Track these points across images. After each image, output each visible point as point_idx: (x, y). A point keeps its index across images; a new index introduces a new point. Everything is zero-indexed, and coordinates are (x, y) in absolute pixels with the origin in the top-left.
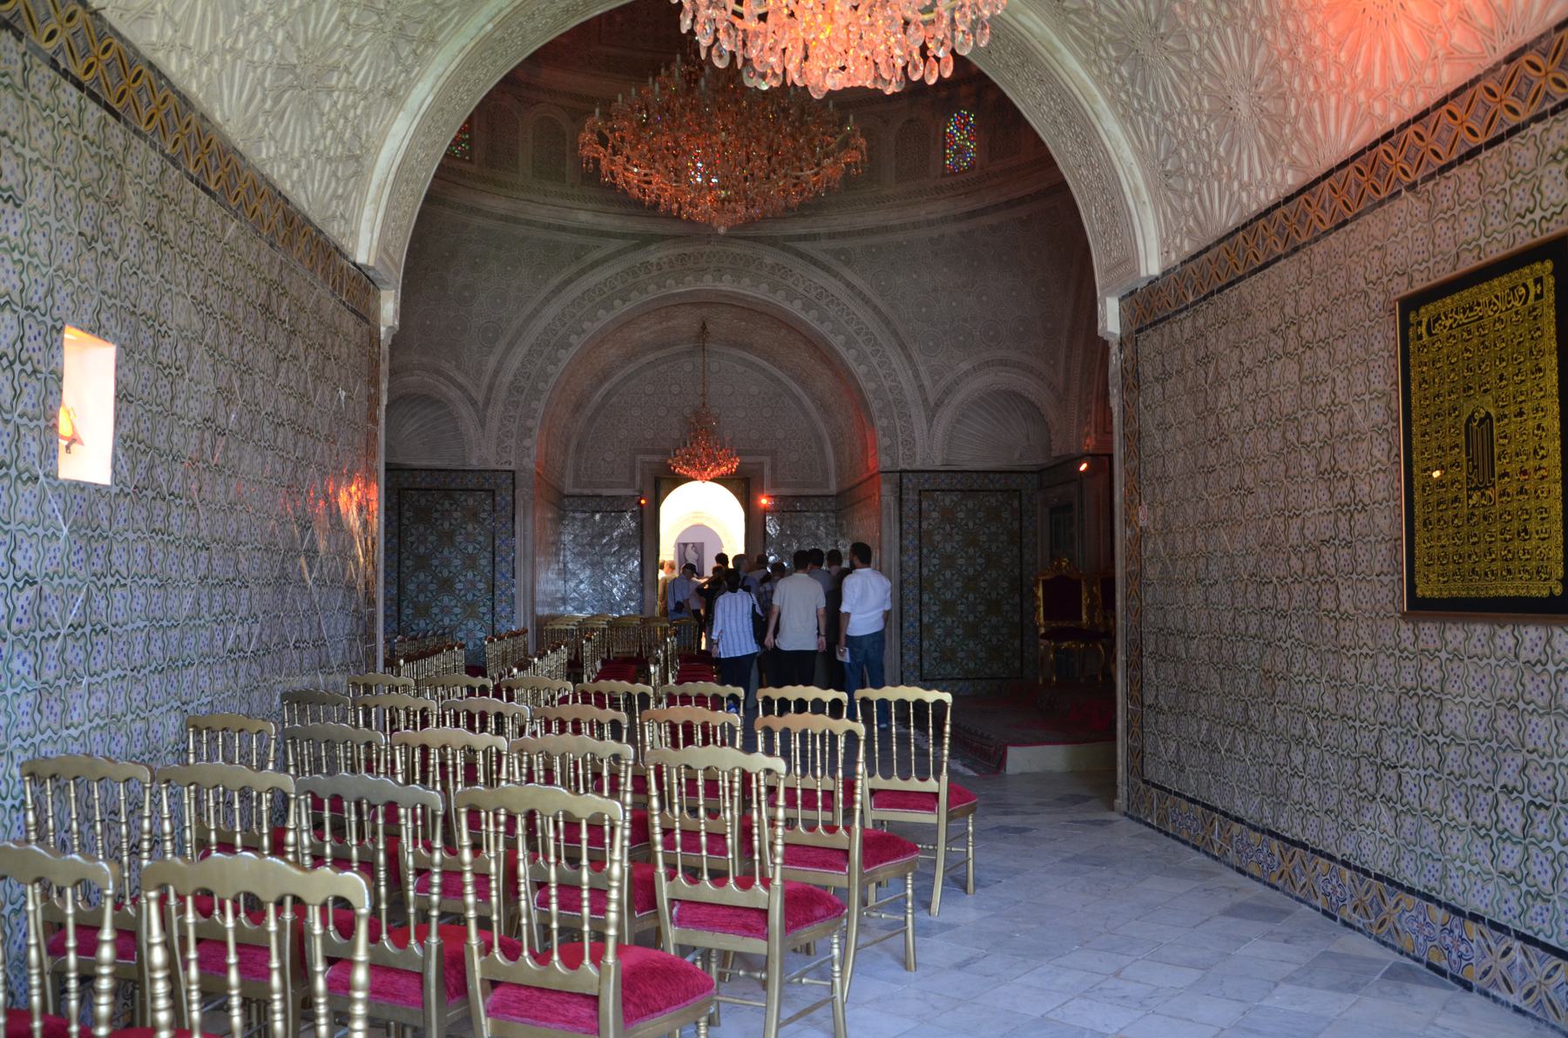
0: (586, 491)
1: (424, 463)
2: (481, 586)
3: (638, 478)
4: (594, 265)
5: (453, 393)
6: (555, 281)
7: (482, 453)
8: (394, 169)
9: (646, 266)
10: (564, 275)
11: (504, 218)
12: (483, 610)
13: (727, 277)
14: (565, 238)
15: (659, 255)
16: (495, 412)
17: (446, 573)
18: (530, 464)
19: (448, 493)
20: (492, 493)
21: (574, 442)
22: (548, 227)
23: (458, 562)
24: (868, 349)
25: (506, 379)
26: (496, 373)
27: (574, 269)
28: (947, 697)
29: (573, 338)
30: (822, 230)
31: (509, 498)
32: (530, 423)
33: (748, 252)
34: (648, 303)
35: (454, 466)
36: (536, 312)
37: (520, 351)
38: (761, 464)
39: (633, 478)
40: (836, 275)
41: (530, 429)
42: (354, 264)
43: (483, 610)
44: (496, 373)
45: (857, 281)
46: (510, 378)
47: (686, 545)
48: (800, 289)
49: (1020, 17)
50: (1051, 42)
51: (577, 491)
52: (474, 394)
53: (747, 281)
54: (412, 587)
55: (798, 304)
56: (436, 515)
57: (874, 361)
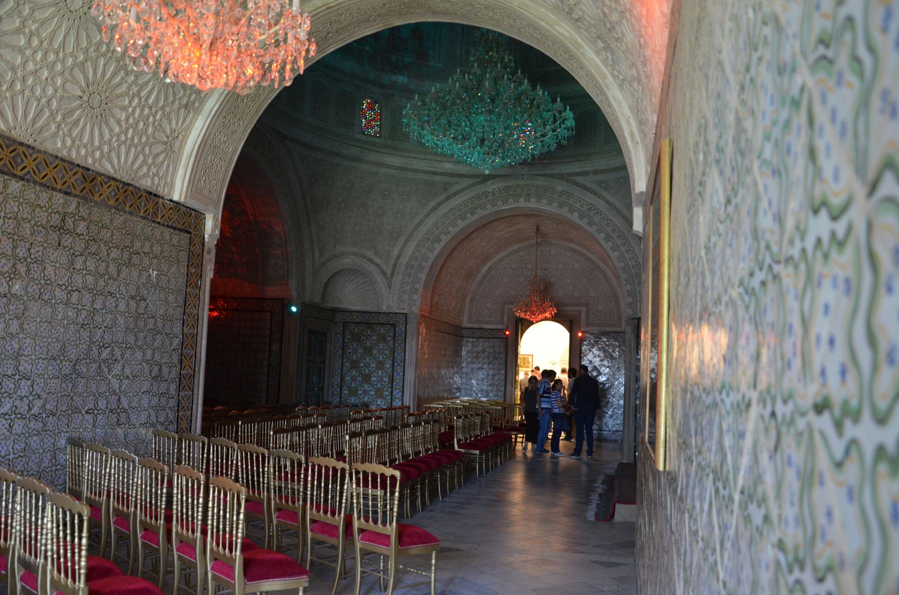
0: (475, 326)
1: (358, 308)
2: (386, 379)
3: (506, 318)
4: (455, 194)
5: (372, 268)
6: (432, 204)
7: (390, 303)
8: (196, 147)
9: (486, 194)
10: (437, 200)
11: (401, 168)
12: (386, 393)
13: (533, 199)
14: (438, 178)
15: (493, 187)
16: (398, 279)
17: (367, 371)
18: (416, 310)
19: (370, 325)
21: (469, 296)
22: (427, 172)
23: (373, 365)
24: (619, 242)
25: (404, 261)
26: (398, 257)
27: (443, 196)
29: (443, 237)
30: (590, 169)
32: (417, 286)
33: (546, 184)
34: (485, 216)
35: (374, 309)
36: (422, 221)
37: (412, 245)
38: (580, 312)
39: (502, 318)
40: (600, 196)
41: (417, 290)
42: (171, 201)
43: (386, 393)
44: (398, 257)
45: (611, 199)
46: (407, 260)
48: (578, 206)
49: (557, 27)
50: (576, 42)
51: (470, 325)
52: (385, 269)
53: (545, 201)
54: (348, 378)
55: (576, 214)
56: (363, 338)
57: (623, 249)
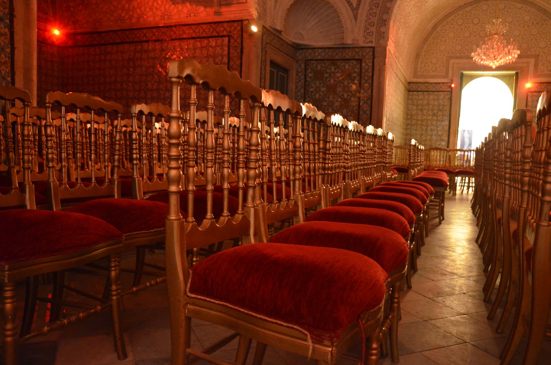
20: (360, 61)
28: (103, 187)
31: (370, 64)
39: (447, 72)
47: (464, 131)
56: (326, 75)
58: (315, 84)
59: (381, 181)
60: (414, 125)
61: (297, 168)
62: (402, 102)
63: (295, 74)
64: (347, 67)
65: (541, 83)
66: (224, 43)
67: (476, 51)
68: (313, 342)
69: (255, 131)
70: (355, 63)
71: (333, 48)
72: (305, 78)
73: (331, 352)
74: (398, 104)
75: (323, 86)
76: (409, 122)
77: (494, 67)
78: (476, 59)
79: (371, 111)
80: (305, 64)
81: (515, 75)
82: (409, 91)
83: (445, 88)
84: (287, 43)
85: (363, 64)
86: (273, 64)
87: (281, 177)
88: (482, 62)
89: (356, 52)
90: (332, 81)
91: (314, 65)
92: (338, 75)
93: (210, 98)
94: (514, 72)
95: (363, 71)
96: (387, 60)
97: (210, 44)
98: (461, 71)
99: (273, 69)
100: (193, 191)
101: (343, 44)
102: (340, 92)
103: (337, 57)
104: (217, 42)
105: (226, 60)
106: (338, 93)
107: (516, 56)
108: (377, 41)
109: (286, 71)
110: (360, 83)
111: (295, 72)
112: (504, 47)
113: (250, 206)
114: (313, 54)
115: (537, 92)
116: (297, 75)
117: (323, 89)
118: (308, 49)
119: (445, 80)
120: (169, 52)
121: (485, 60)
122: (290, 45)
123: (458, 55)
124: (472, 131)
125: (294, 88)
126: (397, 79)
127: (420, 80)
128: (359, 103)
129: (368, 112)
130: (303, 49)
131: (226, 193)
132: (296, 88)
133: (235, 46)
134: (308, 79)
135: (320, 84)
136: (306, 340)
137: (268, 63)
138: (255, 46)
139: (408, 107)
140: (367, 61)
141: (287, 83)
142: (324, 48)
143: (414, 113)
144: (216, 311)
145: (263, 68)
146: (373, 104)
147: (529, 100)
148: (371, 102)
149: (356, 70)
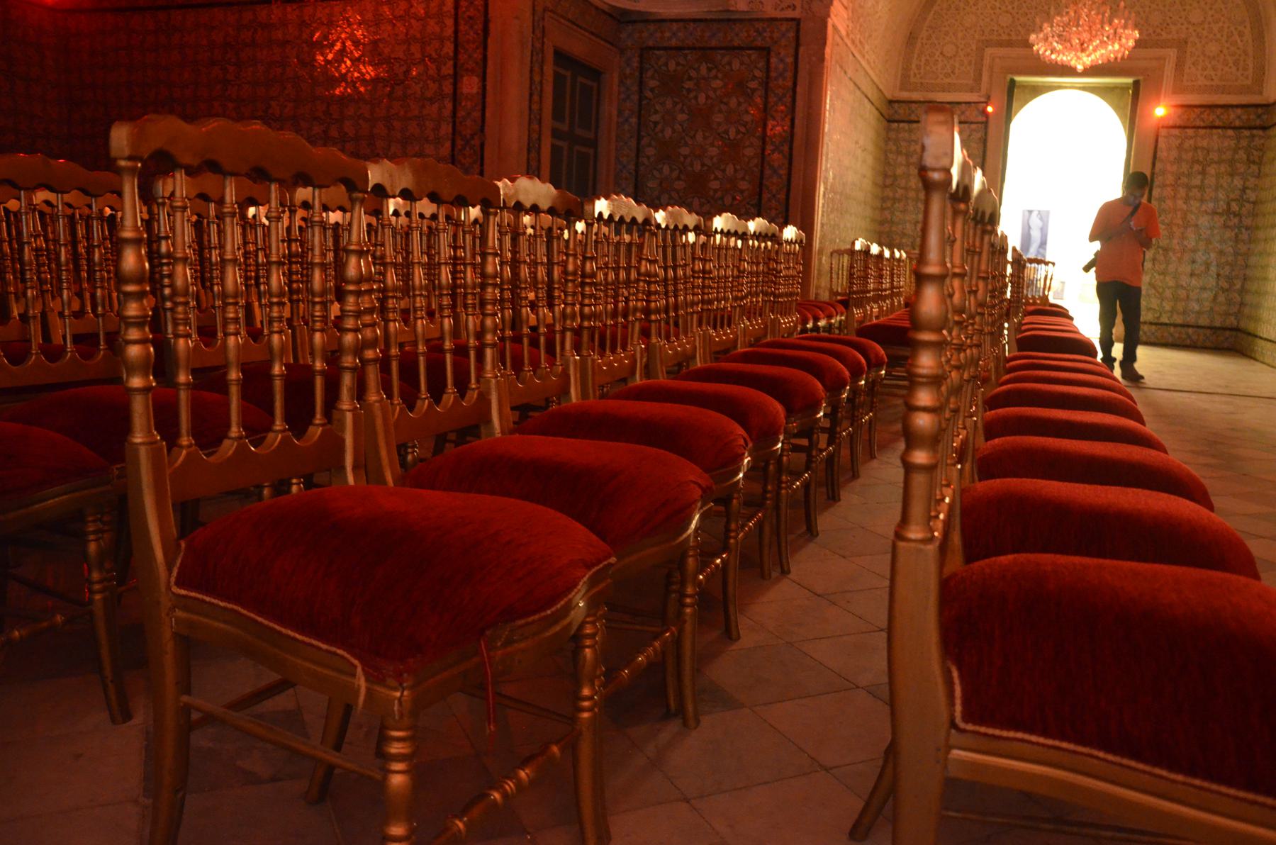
20: (766, 52)
31: (790, 60)
47: (1030, 212)
58: (663, 104)
59: (765, 336)
60: (900, 200)
61: (489, 322)
62: (870, 147)
63: (616, 80)
64: (736, 65)
65: (1182, 106)
66: (445, 9)
67: (1041, 30)
68: (367, 680)
69: (353, 251)
70: (753, 57)
71: (706, 20)
72: (641, 91)
73: (400, 699)
74: (859, 152)
75: (682, 111)
76: (889, 193)
77: (1080, 68)
78: (1040, 48)
79: (790, 170)
80: (641, 56)
81: (1130, 86)
82: (889, 121)
83: (973, 115)
84: (597, 8)
85: (774, 60)
86: (562, 57)
87: (554, 325)
88: (1053, 57)
89: (757, 31)
90: (702, 98)
91: (663, 60)
92: (717, 84)
93: (228, 190)
94: (1130, 80)
95: (773, 74)
96: (828, 50)
97: (413, 10)
98: (1009, 77)
99: (562, 71)
100: (188, 384)
101: (728, 11)
102: (719, 124)
103: (714, 43)
104: (428, 7)
105: (449, 48)
106: (715, 126)
107: (1131, 43)
108: (806, 6)
109: (596, 74)
110: (766, 103)
111: (616, 75)
112: (1102, 23)
113: (345, 407)
114: (658, 35)
115: (1180, 127)
116: (621, 82)
117: (681, 117)
118: (647, 21)
119: (972, 97)
120: (317, 29)
121: (1059, 52)
122: (604, 12)
123: (1005, 37)
124: (1048, 213)
125: (615, 113)
126: (858, 93)
127: (916, 96)
128: (763, 150)
129: (783, 172)
130: (635, 22)
131: (278, 384)
132: (620, 113)
133: (470, 17)
134: (649, 94)
135: (675, 104)
136: (354, 675)
137: (550, 56)
138: (517, 18)
139: (886, 157)
140: (783, 53)
141: (598, 100)
142: (682, 20)
143: (899, 171)
144: (225, 622)
145: (536, 68)
146: (795, 153)
147: (1162, 144)
148: (791, 149)
149: (757, 73)
